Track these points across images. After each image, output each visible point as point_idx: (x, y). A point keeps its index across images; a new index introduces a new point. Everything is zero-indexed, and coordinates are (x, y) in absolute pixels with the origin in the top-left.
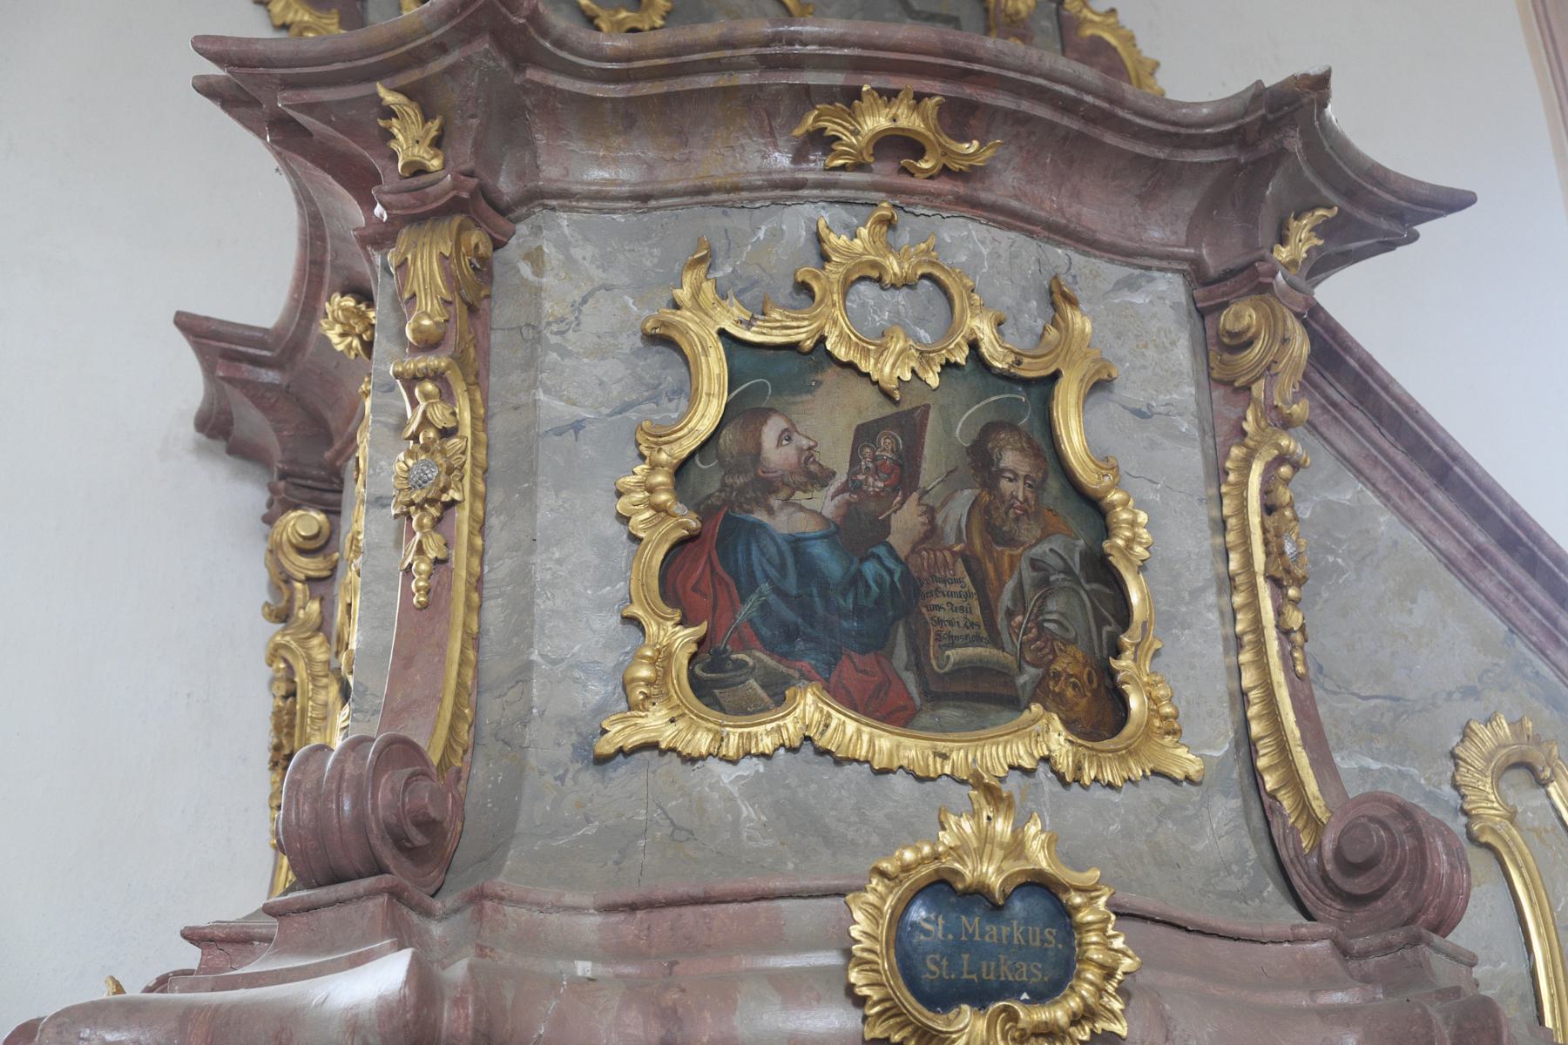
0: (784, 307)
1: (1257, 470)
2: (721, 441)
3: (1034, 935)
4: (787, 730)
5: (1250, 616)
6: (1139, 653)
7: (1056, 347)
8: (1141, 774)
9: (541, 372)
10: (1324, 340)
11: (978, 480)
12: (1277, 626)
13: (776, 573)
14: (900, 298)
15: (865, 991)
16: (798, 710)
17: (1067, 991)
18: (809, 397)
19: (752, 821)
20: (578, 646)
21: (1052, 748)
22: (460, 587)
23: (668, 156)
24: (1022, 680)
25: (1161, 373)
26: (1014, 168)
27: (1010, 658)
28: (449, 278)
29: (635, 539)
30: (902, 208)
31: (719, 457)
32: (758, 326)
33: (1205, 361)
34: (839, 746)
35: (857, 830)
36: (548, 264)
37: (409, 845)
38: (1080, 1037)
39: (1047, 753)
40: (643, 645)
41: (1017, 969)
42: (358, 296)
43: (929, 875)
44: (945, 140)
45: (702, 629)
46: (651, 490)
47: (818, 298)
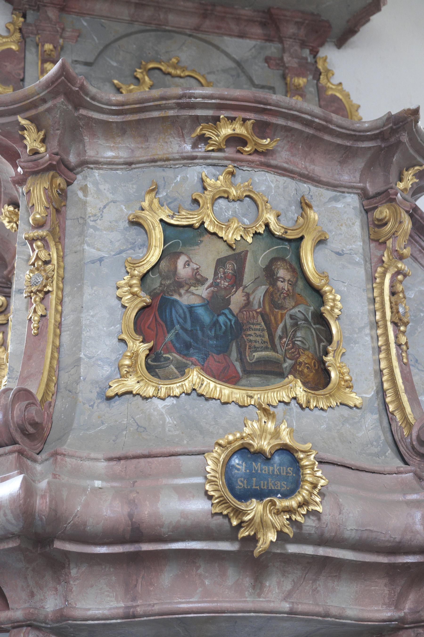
0: (187, 210)
1: (388, 277)
2: (160, 266)
3: (283, 470)
4: (186, 386)
5: (384, 338)
6: (335, 354)
7: (302, 226)
8: (335, 404)
9: (86, 237)
10: (421, 222)
11: (268, 282)
12: (395, 343)
13: (182, 321)
14: (236, 205)
15: (212, 493)
16: (190, 378)
17: (297, 493)
18: (197, 247)
19: (170, 424)
20: (100, 351)
21: (297, 393)
22: (51, 327)
23: (140, 146)
24: (285, 365)
25: (348, 236)
26: (286, 150)
27: (281, 356)
28: (48, 198)
29: (124, 307)
30: (238, 167)
31: (160, 273)
32: (176, 218)
33: (367, 231)
34: (207, 393)
35: (214, 427)
36: (89, 192)
37: (27, 433)
38: (302, 513)
39: (295, 396)
40: (127, 351)
41: (276, 484)
42: (15, 206)
43: (239, 445)
44: (256, 138)
45: (151, 344)
46: (131, 286)
47: (201, 205)
